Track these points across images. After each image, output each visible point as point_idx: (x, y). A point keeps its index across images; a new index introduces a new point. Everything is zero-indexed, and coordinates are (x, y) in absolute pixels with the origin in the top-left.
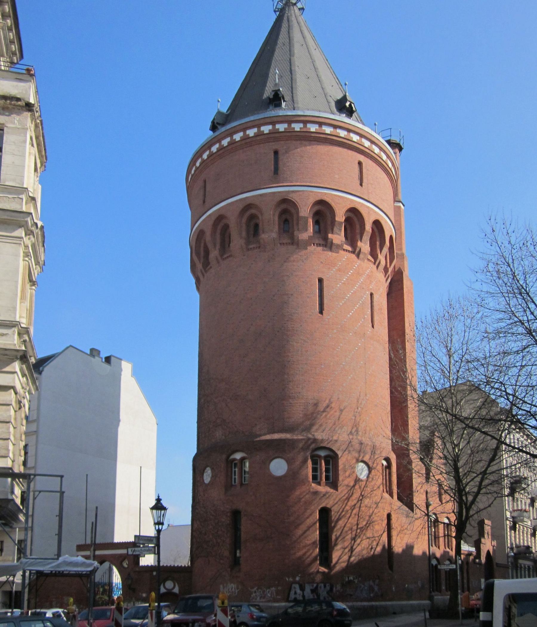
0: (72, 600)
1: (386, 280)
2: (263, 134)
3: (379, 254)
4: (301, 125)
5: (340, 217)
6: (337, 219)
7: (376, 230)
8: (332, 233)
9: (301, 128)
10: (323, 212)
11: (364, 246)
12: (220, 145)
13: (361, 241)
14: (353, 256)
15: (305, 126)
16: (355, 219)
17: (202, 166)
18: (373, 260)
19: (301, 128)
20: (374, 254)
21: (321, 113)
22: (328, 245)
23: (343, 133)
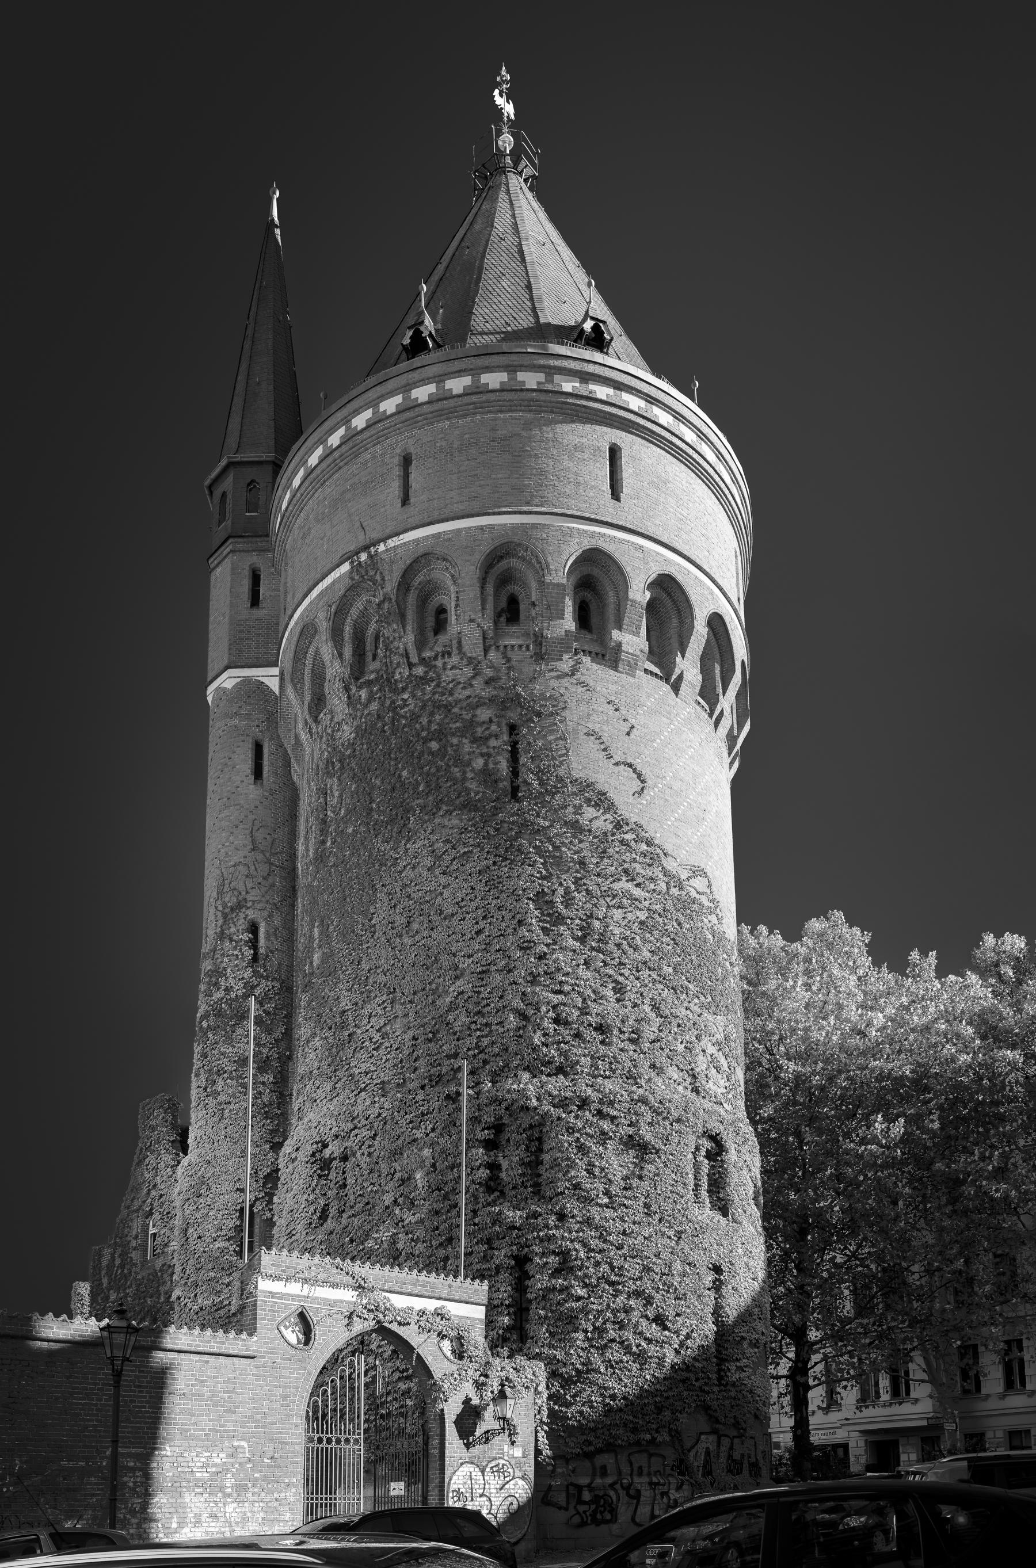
0: (990, 940)
1: (731, 764)
2: (449, 396)
3: (721, 697)
4: (541, 377)
5: (639, 594)
6: (631, 595)
7: (713, 642)
8: (620, 629)
9: (539, 383)
10: (595, 582)
11: (689, 666)
12: (348, 429)
13: (683, 656)
14: (667, 688)
15: (550, 380)
16: (669, 603)
17: (324, 465)
18: (707, 707)
19: (539, 383)
20: (709, 695)
21: (401, 536)
22: (610, 657)
23: (635, 403)
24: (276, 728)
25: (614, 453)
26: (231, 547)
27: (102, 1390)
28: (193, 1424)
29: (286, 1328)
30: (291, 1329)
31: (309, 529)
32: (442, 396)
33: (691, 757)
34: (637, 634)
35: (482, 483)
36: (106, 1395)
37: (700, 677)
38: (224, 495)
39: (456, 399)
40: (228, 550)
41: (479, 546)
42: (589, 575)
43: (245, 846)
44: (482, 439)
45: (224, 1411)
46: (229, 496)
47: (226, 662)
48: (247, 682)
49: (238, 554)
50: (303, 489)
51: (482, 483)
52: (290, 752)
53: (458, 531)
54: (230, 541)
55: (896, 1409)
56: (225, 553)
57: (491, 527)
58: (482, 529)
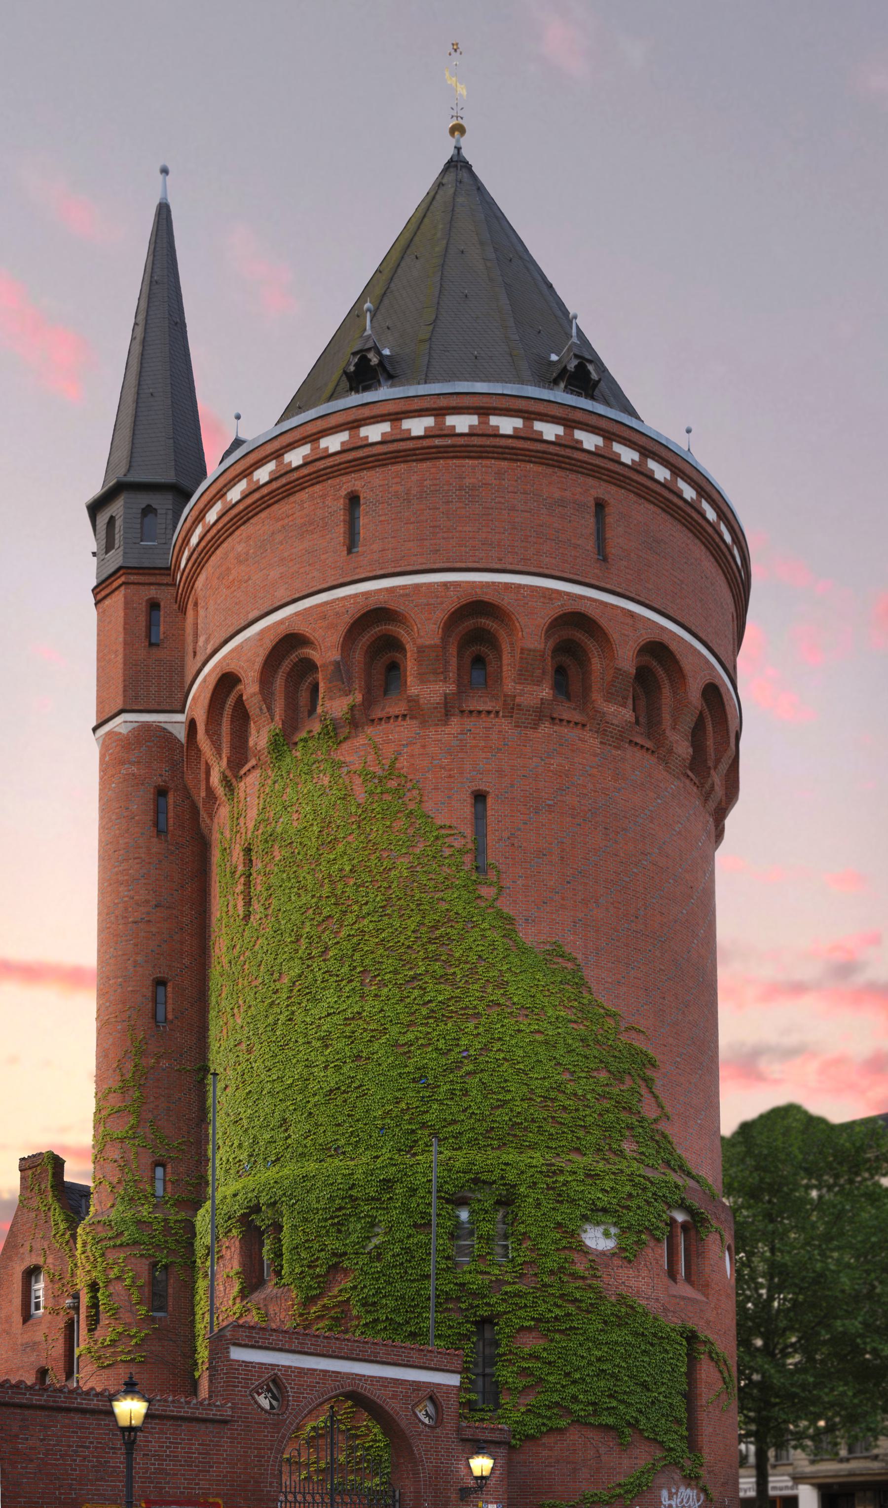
24: (182, 778)
25: (600, 506)
26: (123, 579)
27: (76, 1451)
28: (168, 1483)
29: (259, 1394)
30: (263, 1395)
31: (228, 569)
32: (399, 437)
33: (679, 833)
34: (624, 706)
35: (445, 535)
36: (80, 1456)
37: (691, 750)
38: (112, 520)
39: (414, 442)
40: (120, 581)
41: (442, 603)
42: (352, 492)
43: (147, 901)
44: (445, 488)
45: (199, 1471)
46: (119, 523)
47: (120, 706)
48: (146, 727)
49: (132, 587)
50: (220, 525)
51: (445, 535)
52: (201, 805)
53: (417, 587)
54: (121, 572)
55: (854, 1465)
56: (115, 585)
57: (457, 584)
58: (445, 585)
